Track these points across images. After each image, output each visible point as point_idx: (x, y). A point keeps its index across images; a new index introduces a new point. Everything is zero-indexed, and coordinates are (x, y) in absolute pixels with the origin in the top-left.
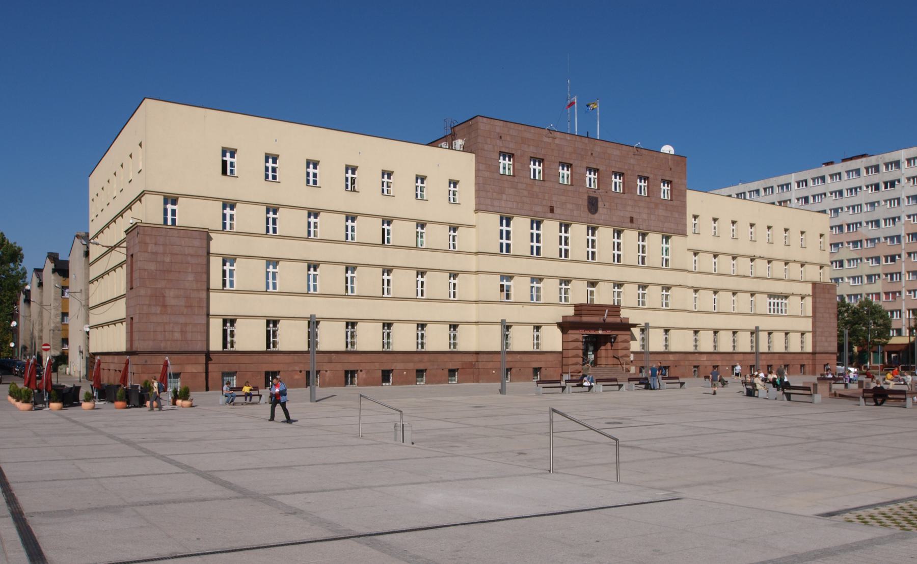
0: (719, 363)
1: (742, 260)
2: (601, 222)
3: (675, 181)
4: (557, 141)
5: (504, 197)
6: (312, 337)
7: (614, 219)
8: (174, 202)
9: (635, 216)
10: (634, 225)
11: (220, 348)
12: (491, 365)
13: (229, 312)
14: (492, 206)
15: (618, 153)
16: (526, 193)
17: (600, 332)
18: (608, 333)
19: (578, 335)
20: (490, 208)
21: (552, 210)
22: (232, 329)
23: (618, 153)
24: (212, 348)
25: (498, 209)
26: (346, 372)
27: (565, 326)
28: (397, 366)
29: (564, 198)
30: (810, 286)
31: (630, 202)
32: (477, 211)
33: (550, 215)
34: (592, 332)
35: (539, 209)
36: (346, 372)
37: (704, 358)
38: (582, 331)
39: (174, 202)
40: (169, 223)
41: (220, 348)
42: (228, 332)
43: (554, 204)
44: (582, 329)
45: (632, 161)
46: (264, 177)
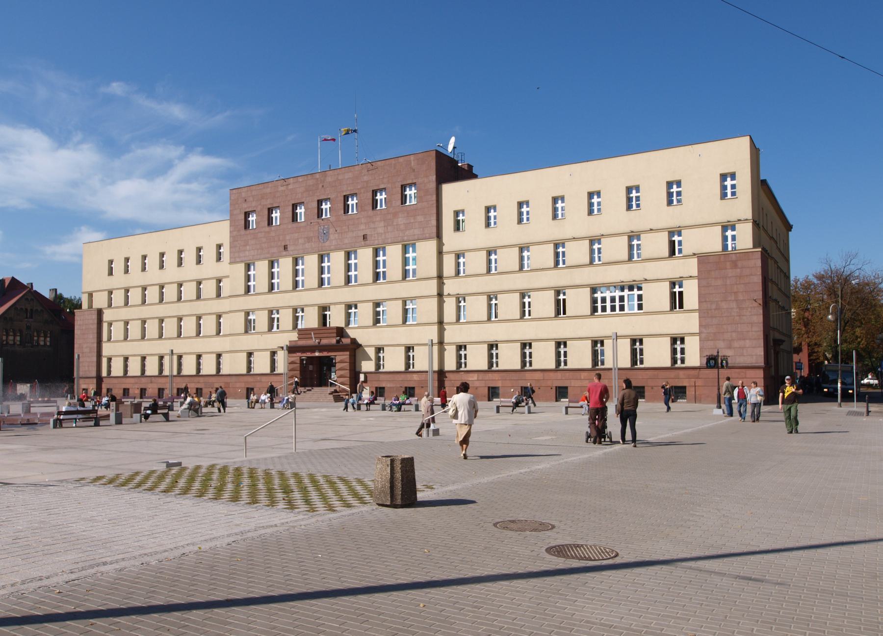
0: (499, 384)
1: (604, 238)
2: (332, 247)
3: (419, 181)
4: (290, 187)
5: (248, 247)
6: (636, 355)
7: (346, 241)
8: (733, 228)
9: (368, 232)
10: (368, 242)
11: (454, 368)
12: (238, 385)
13: (460, 340)
14: (239, 257)
15: (350, 175)
16: (264, 240)
17: (317, 354)
18: (325, 354)
19: (296, 357)
20: (238, 260)
21: (285, 248)
22: (682, 346)
23: (350, 175)
24: (447, 368)
25: (243, 259)
26: (248, 389)
27: (292, 349)
28: (573, 384)
29: (296, 235)
30: (695, 261)
31: (363, 220)
32: (231, 263)
33: (284, 253)
34: (309, 354)
35: (275, 250)
36: (248, 389)
37: (475, 377)
38: (299, 354)
39: (733, 228)
40: (730, 248)
41: (454, 368)
42: (562, 353)
43: (287, 243)
44: (299, 351)
45: (366, 178)
46: (665, 202)
